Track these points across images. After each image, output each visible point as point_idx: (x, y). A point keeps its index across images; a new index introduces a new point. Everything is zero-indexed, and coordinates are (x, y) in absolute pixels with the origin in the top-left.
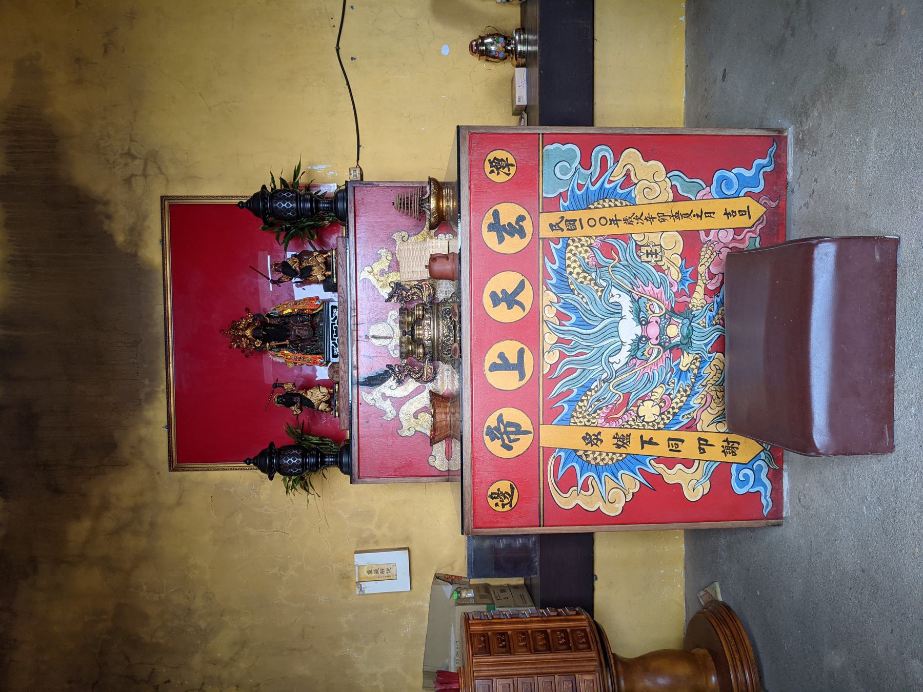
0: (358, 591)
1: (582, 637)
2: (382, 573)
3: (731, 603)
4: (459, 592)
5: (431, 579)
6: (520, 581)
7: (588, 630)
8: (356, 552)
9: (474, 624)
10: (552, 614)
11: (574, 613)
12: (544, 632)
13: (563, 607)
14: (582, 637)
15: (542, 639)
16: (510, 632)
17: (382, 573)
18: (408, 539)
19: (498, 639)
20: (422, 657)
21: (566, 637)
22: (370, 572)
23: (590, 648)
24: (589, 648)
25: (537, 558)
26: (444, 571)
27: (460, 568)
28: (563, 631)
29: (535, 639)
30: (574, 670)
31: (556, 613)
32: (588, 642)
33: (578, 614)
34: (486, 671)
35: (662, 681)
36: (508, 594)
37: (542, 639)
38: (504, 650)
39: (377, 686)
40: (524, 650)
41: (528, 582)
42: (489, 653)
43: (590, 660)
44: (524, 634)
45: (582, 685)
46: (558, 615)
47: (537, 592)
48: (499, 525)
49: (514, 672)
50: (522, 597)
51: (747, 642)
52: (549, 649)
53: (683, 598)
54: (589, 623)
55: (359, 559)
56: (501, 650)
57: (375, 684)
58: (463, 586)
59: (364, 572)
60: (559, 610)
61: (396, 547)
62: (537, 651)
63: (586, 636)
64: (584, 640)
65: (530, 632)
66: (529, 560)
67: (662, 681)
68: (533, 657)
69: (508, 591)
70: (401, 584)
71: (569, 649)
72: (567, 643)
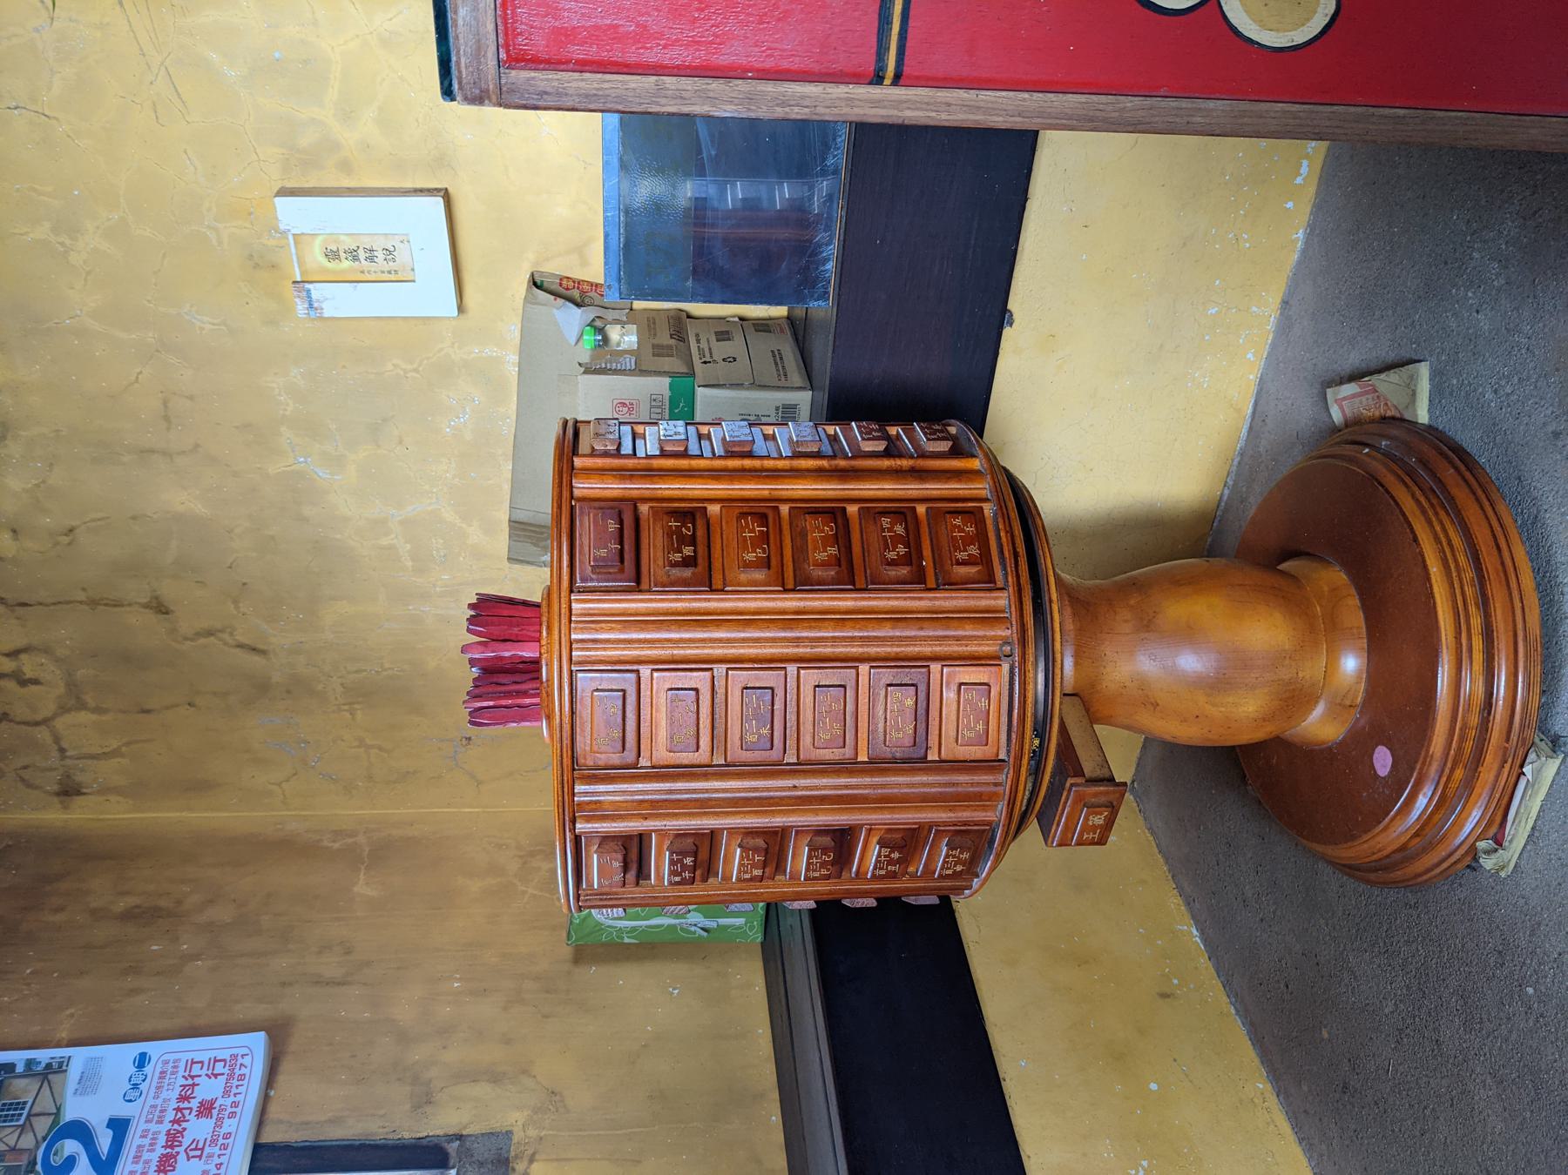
0: (301, 308)
1: (968, 540)
2: (371, 259)
3: (1469, 439)
4: (601, 331)
5: (521, 286)
6: (781, 311)
7: (988, 509)
8: (285, 192)
9: (589, 472)
10: (868, 447)
11: (944, 446)
12: (833, 512)
13: (905, 419)
14: (968, 540)
15: (826, 542)
16: (714, 509)
17: (371, 259)
18: (441, 161)
19: (670, 533)
20: (507, 487)
21: (912, 541)
22: (332, 255)
23: (992, 580)
24: (988, 581)
25: (832, 251)
26: (557, 267)
27: (593, 267)
28: (901, 511)
29: (800, 536)
30: (927, 650)
31: (880, 446)
32: (984, 559)
33: (957, 451)
34: (614, 642)
35: (1190, 662)
36: (735, 347)
37: (826, 542)
38: (687, 573)
39: (391, 547)
40: (759, 575)
41: (799, 311)
42: (637, 584)
43: (988, 618)
44: (762, 518)
45: (950, 695)
46: (887, 454)
47: (822, 349)
48: (652, 56)
49: (719, 652)
50: (777, 357)
51: (1528, 581)
52: (848, 576)
53: (1253, 389)
54: (997, 490)
55: (293, 214)
56: (677, 572)
57: (385, 542)
58: (610, 315)
59: (316, 256)
60: (893, 431)
61: (409, 185)
62: (803, 583)
63: (981, 538)
64: (974, 550)
65: (785, 509)
66: (807, 252)
67: (1190, 662)
68: (791, 602)
69: (738, 339)
70: (430, 293)
71: (918, 579)
72: (912, 558)
